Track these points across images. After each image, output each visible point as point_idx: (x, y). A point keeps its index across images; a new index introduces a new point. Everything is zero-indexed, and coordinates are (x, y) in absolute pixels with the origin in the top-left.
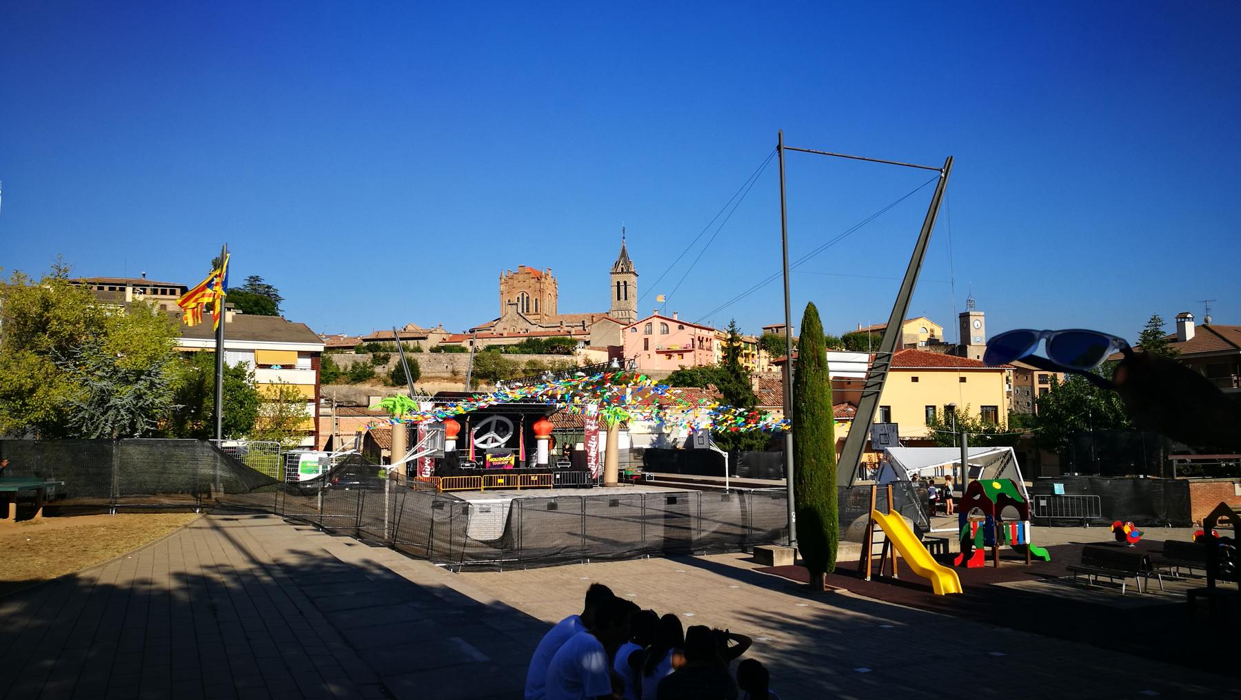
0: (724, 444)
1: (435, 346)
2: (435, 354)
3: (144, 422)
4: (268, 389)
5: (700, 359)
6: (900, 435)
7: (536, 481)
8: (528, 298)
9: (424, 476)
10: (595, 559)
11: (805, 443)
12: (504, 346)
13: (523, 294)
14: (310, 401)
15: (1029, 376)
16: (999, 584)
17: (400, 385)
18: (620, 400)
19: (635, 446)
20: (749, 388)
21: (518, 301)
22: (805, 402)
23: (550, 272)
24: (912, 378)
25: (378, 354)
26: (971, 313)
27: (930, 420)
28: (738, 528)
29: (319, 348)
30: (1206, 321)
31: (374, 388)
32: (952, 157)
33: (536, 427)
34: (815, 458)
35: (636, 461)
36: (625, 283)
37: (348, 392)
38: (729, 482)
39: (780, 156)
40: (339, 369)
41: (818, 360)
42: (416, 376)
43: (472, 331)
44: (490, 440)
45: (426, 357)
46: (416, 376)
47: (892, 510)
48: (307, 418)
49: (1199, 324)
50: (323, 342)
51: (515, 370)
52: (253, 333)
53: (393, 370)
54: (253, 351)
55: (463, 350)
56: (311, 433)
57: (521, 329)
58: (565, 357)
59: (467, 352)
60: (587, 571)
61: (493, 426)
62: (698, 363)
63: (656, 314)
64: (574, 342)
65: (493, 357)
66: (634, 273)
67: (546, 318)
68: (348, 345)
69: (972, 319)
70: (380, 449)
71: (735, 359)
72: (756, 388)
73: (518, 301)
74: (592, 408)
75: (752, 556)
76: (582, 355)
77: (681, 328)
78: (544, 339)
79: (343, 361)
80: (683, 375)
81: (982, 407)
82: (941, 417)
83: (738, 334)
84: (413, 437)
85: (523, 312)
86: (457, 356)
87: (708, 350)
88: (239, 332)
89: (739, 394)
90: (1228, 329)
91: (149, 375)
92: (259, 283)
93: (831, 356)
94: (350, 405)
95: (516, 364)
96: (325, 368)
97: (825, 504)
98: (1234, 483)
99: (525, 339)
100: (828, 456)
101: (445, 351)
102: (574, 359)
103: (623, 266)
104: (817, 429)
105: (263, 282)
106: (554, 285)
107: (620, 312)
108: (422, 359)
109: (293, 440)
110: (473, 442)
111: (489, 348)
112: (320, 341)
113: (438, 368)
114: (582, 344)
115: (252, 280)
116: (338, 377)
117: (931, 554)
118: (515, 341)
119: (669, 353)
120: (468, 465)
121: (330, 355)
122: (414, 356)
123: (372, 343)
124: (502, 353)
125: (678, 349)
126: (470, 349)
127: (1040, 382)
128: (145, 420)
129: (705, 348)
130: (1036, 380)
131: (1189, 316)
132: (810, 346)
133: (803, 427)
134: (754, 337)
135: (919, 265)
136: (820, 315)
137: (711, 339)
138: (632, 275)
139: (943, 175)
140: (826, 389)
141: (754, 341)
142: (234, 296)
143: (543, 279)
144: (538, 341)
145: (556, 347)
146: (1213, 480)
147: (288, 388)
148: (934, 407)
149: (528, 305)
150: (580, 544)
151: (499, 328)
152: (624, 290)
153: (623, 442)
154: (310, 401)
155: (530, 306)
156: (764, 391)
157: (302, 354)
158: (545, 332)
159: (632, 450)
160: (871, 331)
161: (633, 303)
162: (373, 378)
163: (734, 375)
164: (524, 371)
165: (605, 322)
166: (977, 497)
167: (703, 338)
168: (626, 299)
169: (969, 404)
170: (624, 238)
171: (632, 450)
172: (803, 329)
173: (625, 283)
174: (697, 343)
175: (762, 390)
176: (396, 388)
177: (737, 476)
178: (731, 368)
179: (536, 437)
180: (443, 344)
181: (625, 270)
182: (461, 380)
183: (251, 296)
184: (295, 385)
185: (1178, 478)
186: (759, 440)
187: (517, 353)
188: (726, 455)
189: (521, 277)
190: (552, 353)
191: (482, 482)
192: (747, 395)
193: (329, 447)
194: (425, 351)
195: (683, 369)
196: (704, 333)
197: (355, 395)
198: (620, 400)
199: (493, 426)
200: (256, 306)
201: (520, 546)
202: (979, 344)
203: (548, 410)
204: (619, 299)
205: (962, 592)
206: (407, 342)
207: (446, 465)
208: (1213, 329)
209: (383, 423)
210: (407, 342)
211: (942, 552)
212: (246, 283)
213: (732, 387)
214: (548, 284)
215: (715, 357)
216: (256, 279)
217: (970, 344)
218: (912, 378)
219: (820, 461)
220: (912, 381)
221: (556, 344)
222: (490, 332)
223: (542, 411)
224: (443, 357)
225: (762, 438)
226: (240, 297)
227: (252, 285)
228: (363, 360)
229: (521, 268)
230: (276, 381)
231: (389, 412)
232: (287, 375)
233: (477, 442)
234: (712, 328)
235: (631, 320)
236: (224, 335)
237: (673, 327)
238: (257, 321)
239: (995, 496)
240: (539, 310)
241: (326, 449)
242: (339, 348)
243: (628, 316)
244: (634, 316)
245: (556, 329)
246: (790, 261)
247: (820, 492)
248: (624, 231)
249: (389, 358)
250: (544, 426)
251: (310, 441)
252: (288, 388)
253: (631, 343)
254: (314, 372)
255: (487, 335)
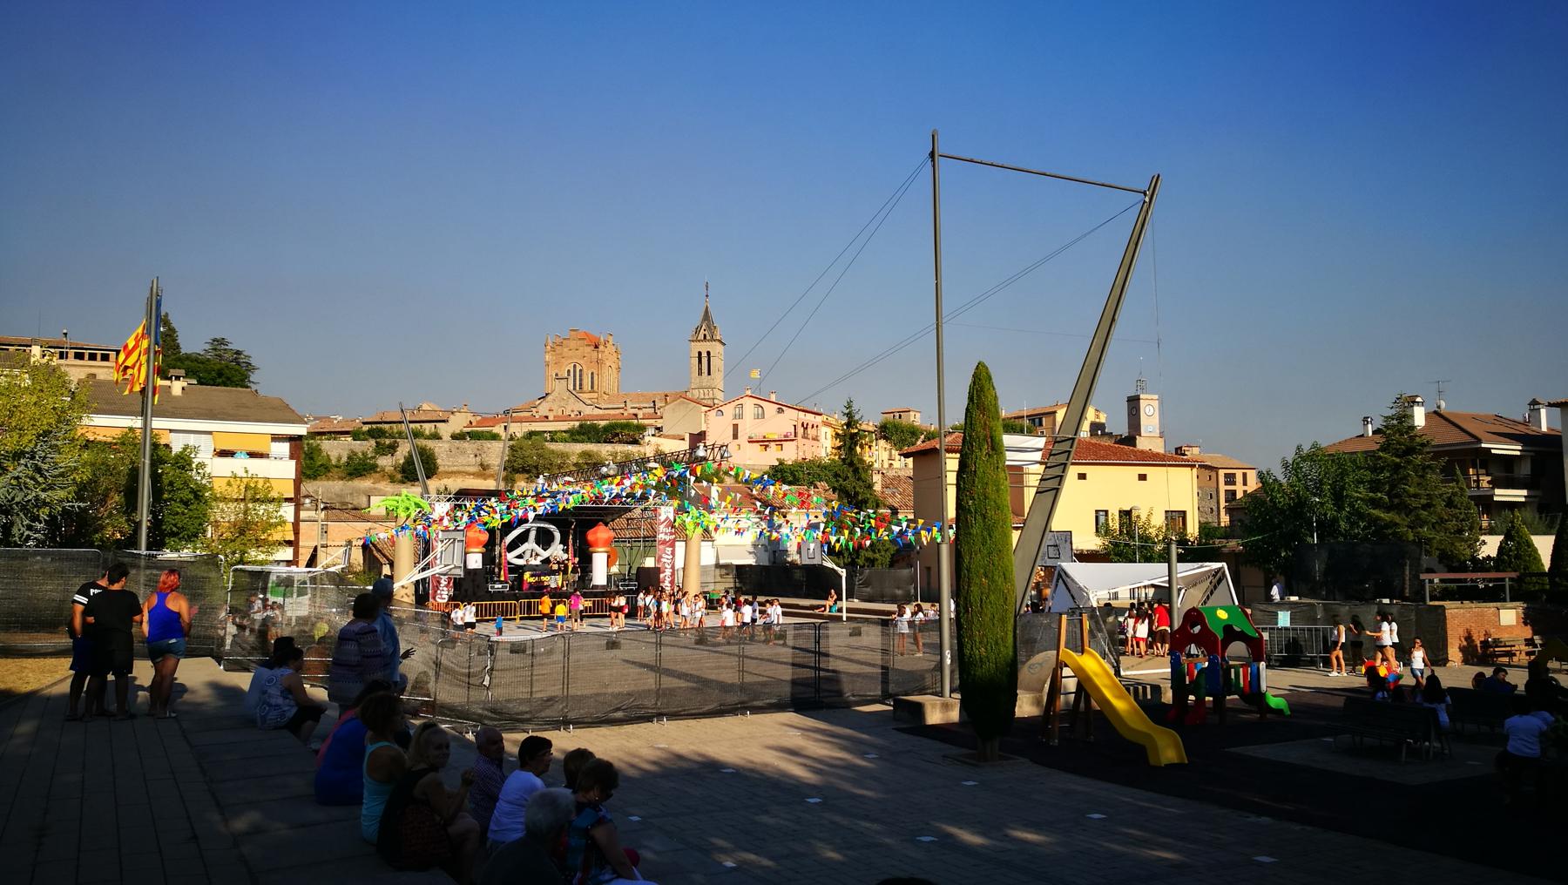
0: (839, 558)
1: (458, 431)
2: (457, 441)
3: (23, 526)
4: (229, 484)
5: (804, 452)
6: (1074, 547)
7: (590, 607)
8: (581, 370)
9: (440, 601)
10: (674, 716)
11: (973, 556)
12: (550, 432)
13: (575, 366)
14: (287, 500)
15: (1213, 474)
16: (1233, 750)
17: (411, 481)
18: (704, 502)
19: (722, 562)
20: (870, 486)
21: (569, 375)
22: (973, 499)
23: (611, 338)
24: (1079, 474)
25: (382, 440)
26: (1141, 396)
27: (1101, 528)
28: (834, 654)
29: (301, 430)
30: (1439, 407)
31: (377, 486)
32: (1159, 176)
33: (591, 536)
34: (986, 577)
35: (724, 580)
36: (708, 353)
37: (342, 490)
38: (847, 609)
39: (934, 166)
40: (330, 460)
41: (992, 440)
42: (431, 470)
43: (506, 412)
44: (528, 554)
45: (446, 446)
46: (431, 470)
47: (1086, 648)
48: (283, 522)
49: (1429, 411)
50: (306, 423)
51: (564, 464)
52: (211, 410)
53: (402, 461)
54: (210, 433)
55: (495, 437)
56: (289, 543)
57: (572, 411)
58: (630, 448)
59: (500, 440)
60: (664, 735)
61: (533, 535)
62: (801, 456)
63: (749, 393)
64: (642, 428)
65: (534, 446)
66: (719, 341)
67: (606, 397)
68: (343, 430)
69: (1143, 404)
70: (382, 564)
71: (853, 449)
72: (877, 488)
73: (569, 375)
74: (667, 512)
75: (892, 708)
76: (650, 445)
77: (780, 411)
78: (603, 423)
79: (336, 450)
80: (782, 471)
81: (1166, 512)
82: (1115, 524)
83: (856, 418)
84: (426, 548)
85: (574, 389)
86: (487, 444)
87: (813, 439)
88: (191, 408)
89: (857, 494)
90: (1464, 417)
91: (33, 458)
92: (226, 347)
93: (1008, 440)
94: (344, 507)
95: (564, 455)
96: (312, 458)
97: (1000, 641)
98: (1498, 609)
99: (577, 424)
100: (1004, 574)
101: (471, 438)
102: (642, 449)
103: (706, 332)
104: (991, 536)
105: (230, 347)
106: (615, 354)
107: (701, 391)
108: (441, 449)
109: (263, 553)
110: (505, 556)
111: (531, 434)
112: (299, 420)
113: (462, 460)
114: (651, 431)
115: (216, 343)
116: (329, 471)
117: (1135, 700)
118: (564, 426)
119: (765, 443)
120: (500, 586)
121: (319, 442)
122: (430, 444)
123: (374, 426)
124: (548, 441)
125: (776, 437)
126: (503, 434)
127: (1226, 483)
128: (25, 523)
129: (810, 437)
130: (1222, 480)
131: (1419, 399)
132: (980, 422)
133: (970, 534)
134: (871, 424)
135: (1113, 320)
136: (994, 380)
137: (817, 426)
138: (717, 343)
139: (1147, 199)
140: (1002, 481)
141: (871, 429)
142: (190, 363)
143: (601, 348)
144: (594, 427)
145: (617, 435)
146: (1473, 605)
147: (256, 482)
148: (1106, 512)
149: (581, 380)
150: (654, 686)
151: (543, 409)
152: (706, 362)
153: (707, 555)
154: (287, 500)
155: (585, 382)
156: (888, 491)
157: (276, 438)
158: (604, 415)
159: (718, 566)
160: (1027, 416)
161: (718, 378)
162: (377, 472)
163: (851, 469)
164: (575, 465)
165: (684, 403)
166: (1197, 629)
167: (807, 424)
168: (709, 374)
169: (1152, 509)
170: (707, 296)
171: (718, 566)
172: (971, 399)
173: (708, 353)
174: (800, 431)
175: (885, 489)
176: (405, 485)
177: (855, 600)
178: (848, 461)
179: (591, 549)
180: (469, 430)
181: (708, 337)
182: (491, 476)
183: (214, 364)
184: (267, 480)
185: (1431, 603)
186: (883, 553)
187: (566, 441)
188: (843, 572)
189: (573, 344)
190: (612, 442)
191: (518, 609)
192: (868, 496)
193: (312, 562)
194: (444, 438)
195: (781, 463)
196: (810, 417)
197: (351, 494)
198: (704, 502)
199: (533, 535)
200: (220, 377)
201: (565, 693)
202: (1152, 435)
203: (609, 514)
204: (700, 373)
205: (1186, 762)
206: (421, 426)
207: (468, 587)
208: (1447, 416)
209: (382, 534)
210: (421, 426)
211: (1149, 697)
212: (208, 347)
213: (848, 485)
214: (607, 353)
215: (825, 447)
216: (222, 342)
217: (1140, 435)
218: (1079, 474)
219: (993, 581)
220: (1079, 479)
221: (618, 431)
222: (531, 413)
223: (600, 515)
224: (469, 446)
225: (886, 551)
226: (200, 365)
227: (215, 349)
228: (362, 448)
229: (572, 333)
230: (241, 473)
231: (390, 516)
232: (256, 466)
233: (511, 557)
234: (819, 412)
235: (716, 401)
236: (152, 410)
237: (770, 409)
238: (219, 395)
239: (1221, 629)
240: (596, 387)
241: (308, 565)
242: (330, 433)
243: (711, 396)
244: (720, 395)
245: (618, 411)
246: (945, 310)
247: (993, 625)
248: (707, 287)
249: (398, 447)
250: (600, 533)
251: (287, 554)
252: (256, 482)
253: (718, 430)
254: (293, 462)
255: (528, 417)
